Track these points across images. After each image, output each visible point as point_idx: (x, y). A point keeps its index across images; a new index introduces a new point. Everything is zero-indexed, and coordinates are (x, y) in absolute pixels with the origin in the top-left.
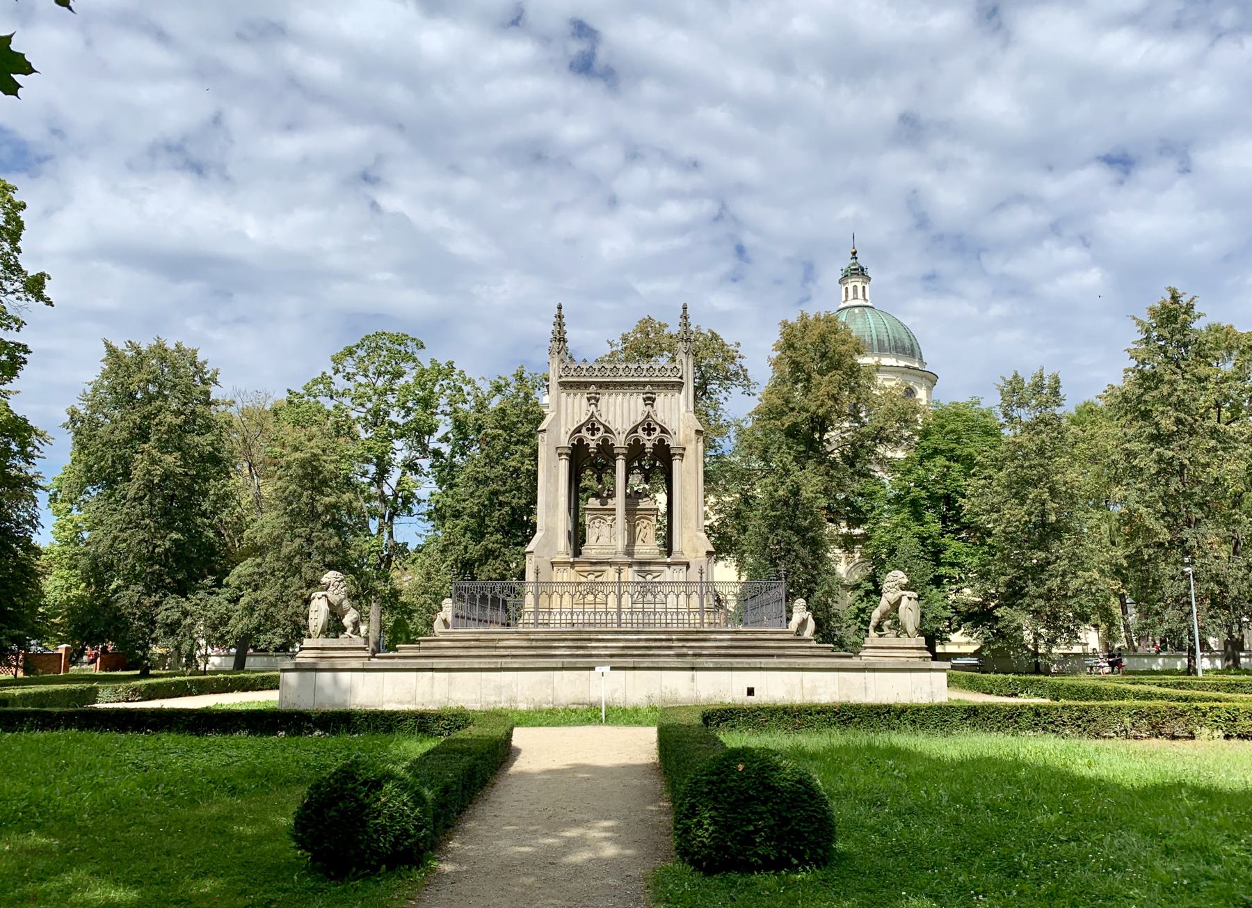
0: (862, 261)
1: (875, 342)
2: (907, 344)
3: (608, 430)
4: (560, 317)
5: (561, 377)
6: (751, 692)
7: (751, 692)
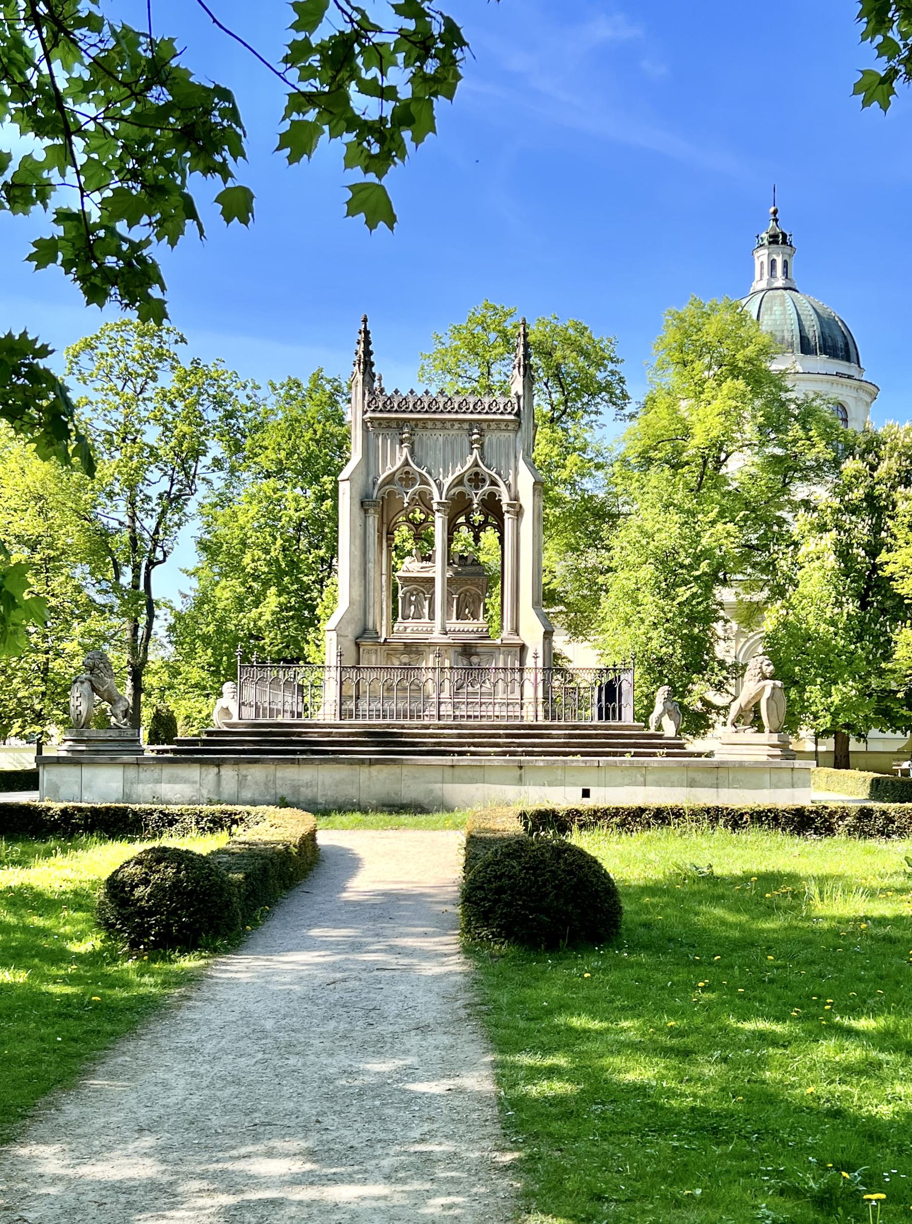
1: (797, 340)
2: (840, 344)
3: (494, 483)
5: (365, 412)
6: (586, 793)
7: (586, 793)
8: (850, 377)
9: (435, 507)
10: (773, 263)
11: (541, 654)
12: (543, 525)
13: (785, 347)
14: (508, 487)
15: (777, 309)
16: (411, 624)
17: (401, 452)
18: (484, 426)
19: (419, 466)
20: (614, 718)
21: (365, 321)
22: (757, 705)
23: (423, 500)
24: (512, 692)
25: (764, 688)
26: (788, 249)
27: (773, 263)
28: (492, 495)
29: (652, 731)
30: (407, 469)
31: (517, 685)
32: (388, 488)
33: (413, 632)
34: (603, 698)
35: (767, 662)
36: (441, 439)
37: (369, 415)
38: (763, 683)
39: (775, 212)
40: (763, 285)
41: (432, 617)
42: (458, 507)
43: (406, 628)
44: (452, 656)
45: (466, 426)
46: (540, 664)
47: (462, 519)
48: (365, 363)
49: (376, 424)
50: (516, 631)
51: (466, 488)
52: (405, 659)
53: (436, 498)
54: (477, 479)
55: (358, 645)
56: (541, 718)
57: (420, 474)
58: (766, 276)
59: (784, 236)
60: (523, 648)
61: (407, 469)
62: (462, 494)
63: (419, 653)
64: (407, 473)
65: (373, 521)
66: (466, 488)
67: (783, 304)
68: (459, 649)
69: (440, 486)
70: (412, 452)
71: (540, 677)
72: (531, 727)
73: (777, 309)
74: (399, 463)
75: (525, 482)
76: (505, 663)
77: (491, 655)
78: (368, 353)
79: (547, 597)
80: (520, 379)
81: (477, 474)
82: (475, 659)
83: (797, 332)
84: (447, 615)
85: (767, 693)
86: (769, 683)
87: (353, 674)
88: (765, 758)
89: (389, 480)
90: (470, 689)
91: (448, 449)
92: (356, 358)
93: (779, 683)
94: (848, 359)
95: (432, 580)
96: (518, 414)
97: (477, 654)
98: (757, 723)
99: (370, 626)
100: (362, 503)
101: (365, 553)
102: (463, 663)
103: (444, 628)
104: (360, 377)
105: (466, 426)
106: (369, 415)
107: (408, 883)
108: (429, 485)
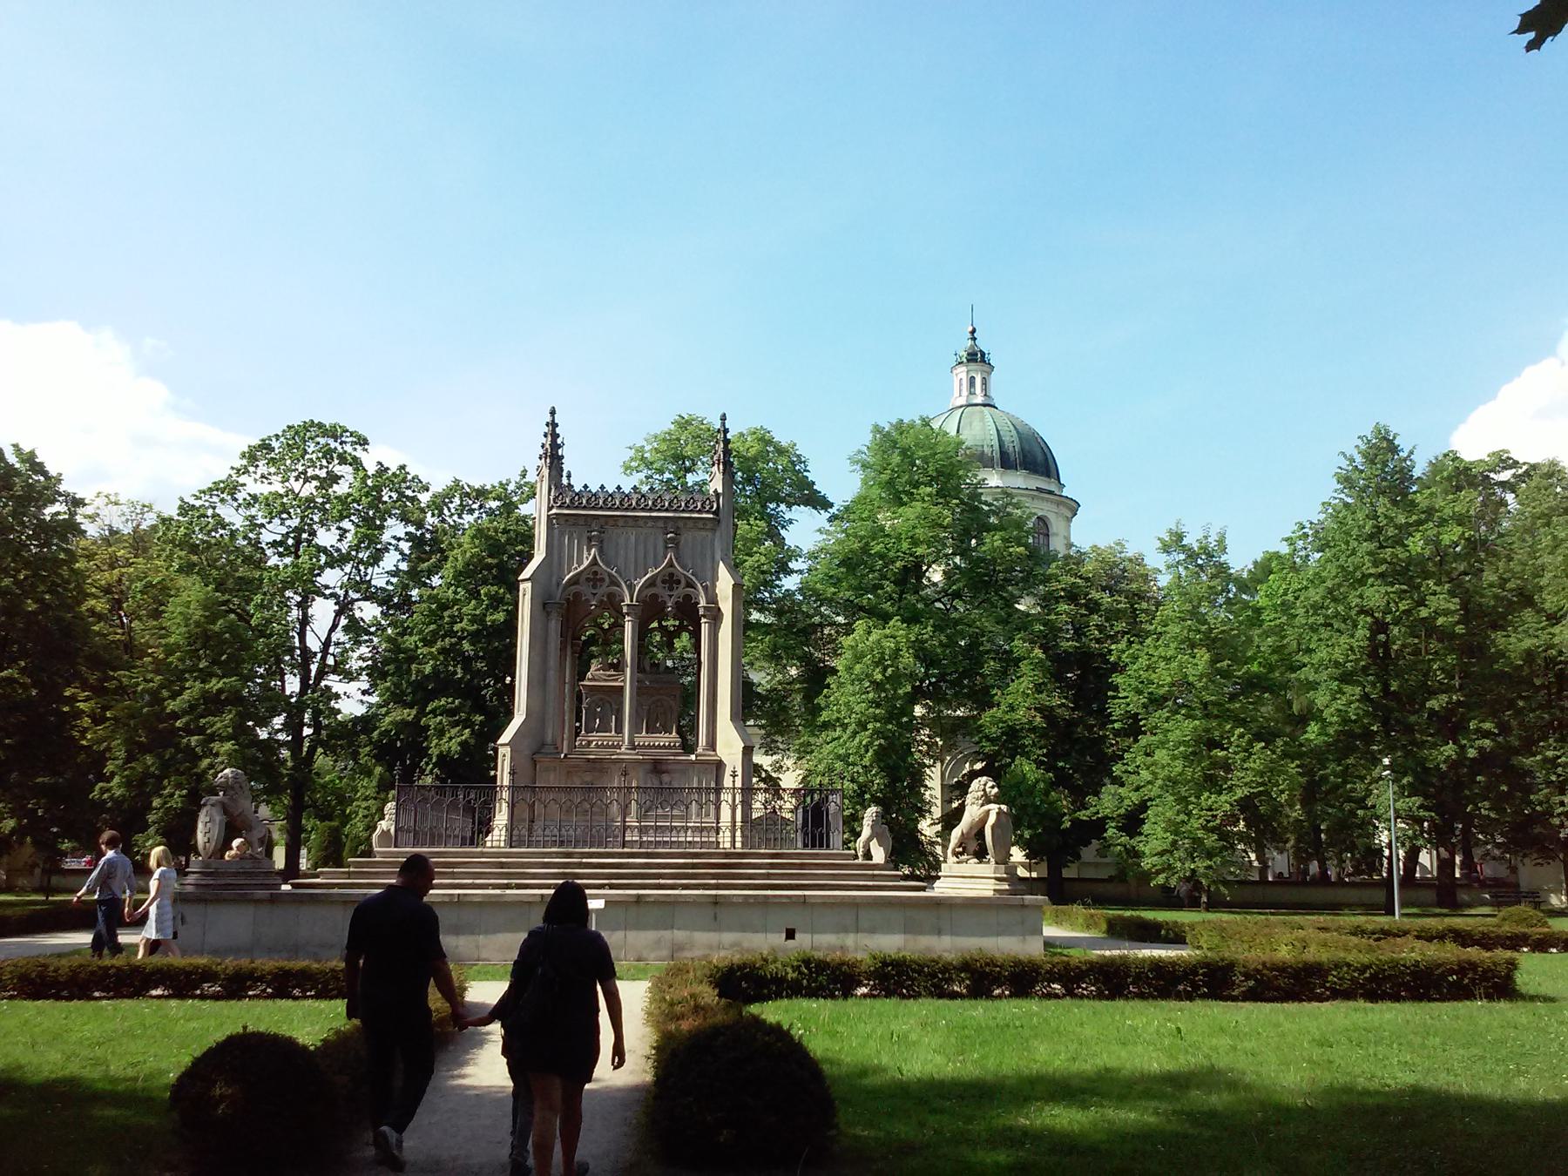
0: (982, 344)
1: (997, 455)
2: (1040, 458)
3: (690, 585)
4: (554, 425)
5: (550, 509)
8: (1051, 492)
9: (625, 610)
10: (972, 381)
11: (739, 772)
12: (744, 628)
13: (987, 462)
14: (705, 589)
15: (977, 425)
16: (595, 738)
17: (589, 551)
18: (681, 524)
19: (608, 565)
20: (821, 846)
21: (553, 412)
22: (980, 834)
23: (613, 603)
24: (708, 815)
25: (988, 812)
26: (986, 368)
27: (972, 381)
28: (688, 597)
29: (860, 861)
30: (595, 568)
31: (712, 807)
32: (574, 589)
33: (597, 746)
34: (738, 839)
35: (990, 784)
36: (633, 538)
37: (554, 511)
38: (986, 807)
39: (973, 331)
40: (962, 401)
41: (619, 730)
42: (650, 609)
43: (590, 742)
44: (641, 775)
45: (661, 524)
46: (739, 784)
47: (655, 625)
48: (552, 456)
49: (562, 521)
50: (712, 745)
51: (659, 590)
52: (588, 778)
53: (627, 601)
54: (671, 580)
55: (535, 763)
56: (738, 845)
57: (610, 575)
58: (965, 392)
59: (983, 354)
60: (720, 765)
61: (595, 568)
62: (654, 596)
63: (603, 771)
64: (595, 573)
65: (555, 625)
66: (659, 590)
67: (982, 419)
68: (648, 767)
69: (631, 588)
70: (601, 551)
71: (738, 798)
72: (727, 855)
73: (977, 425)
74: (586, 563)
75: (725, 583)
76: (700, 782)
77: (684, 772)
78: (555, 446)
79: (748, 701)
80: (719, 477)
81: (671, 575)
82: (666, 778)
83: (996, 447)
84: (636, 729)
85: (992, 819)
86: (994, 807)
87: (528, 795)
88: (990, 894)
89: (575, 581)
90: (660, 811)
91: (641, 547)
92: (541, 452)
93: (1004, 807)
94: (1048, 476)
95: (621, 689)
96: (716, 513)
97: (667, 772)
98: (981, 854)
99: (549, 739)
100: (544, 605)
101: (545, 660)
102: (653, 782)
103: (631, 742)
104: (546, 472)
105: (661, 524)
106: (554, 511)
107: (734, 837)
108: (619, 586)
